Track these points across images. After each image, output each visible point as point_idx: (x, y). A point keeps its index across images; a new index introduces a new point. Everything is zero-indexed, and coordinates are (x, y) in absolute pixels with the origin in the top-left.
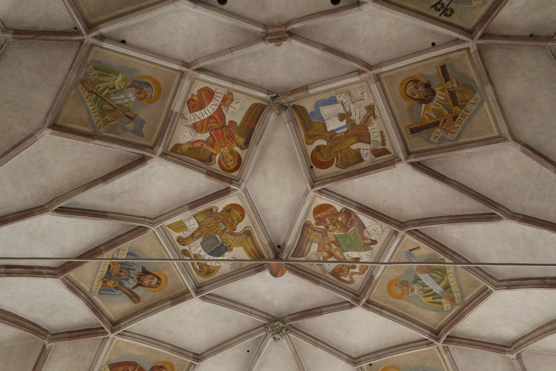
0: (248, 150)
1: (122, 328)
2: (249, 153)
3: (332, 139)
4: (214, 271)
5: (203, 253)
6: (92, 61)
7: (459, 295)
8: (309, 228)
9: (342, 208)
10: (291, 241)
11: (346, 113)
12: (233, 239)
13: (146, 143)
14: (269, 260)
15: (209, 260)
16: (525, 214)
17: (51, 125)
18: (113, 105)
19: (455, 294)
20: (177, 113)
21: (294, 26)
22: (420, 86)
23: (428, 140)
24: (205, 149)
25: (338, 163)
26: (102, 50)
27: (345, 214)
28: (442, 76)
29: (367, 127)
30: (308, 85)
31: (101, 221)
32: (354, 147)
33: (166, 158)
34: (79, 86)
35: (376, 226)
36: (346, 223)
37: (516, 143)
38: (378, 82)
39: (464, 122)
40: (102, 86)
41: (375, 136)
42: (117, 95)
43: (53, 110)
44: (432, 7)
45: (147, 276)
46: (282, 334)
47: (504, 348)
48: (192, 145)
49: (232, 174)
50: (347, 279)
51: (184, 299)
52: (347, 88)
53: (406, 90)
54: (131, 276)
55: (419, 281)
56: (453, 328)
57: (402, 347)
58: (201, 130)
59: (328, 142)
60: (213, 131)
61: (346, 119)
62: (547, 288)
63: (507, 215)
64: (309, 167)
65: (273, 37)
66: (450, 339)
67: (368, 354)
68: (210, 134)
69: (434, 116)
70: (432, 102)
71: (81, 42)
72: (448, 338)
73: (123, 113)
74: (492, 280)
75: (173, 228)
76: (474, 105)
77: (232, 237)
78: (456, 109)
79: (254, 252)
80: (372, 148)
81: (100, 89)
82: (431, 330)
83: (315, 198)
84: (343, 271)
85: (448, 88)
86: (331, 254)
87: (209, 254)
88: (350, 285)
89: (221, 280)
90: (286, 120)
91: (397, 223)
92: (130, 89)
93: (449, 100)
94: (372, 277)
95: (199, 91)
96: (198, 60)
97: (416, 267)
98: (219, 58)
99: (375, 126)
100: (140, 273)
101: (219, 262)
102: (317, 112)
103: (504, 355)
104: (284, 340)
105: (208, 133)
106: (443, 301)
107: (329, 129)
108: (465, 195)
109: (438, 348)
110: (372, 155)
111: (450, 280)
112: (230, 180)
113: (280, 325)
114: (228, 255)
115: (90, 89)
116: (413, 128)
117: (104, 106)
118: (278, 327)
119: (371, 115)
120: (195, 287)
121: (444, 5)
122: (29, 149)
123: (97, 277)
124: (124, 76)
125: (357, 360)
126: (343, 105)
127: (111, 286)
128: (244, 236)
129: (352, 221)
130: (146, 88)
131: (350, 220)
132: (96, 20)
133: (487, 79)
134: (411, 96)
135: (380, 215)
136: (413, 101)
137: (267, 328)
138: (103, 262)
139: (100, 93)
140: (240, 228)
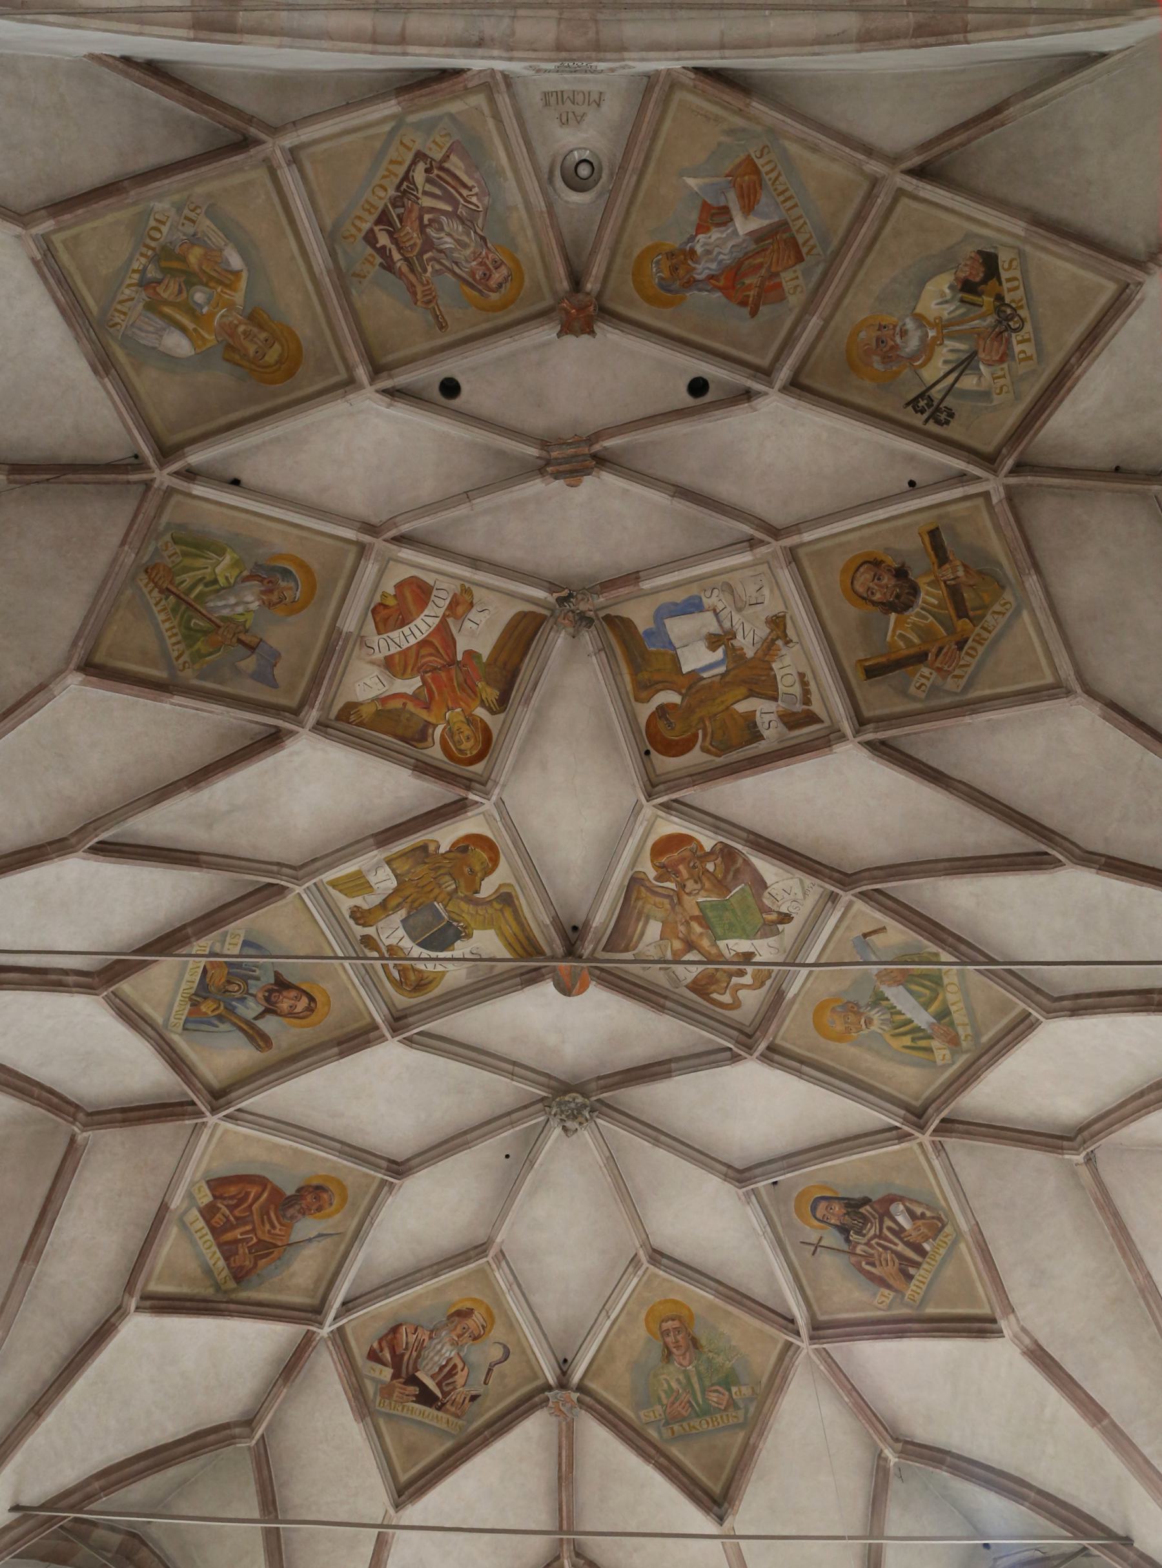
2: (508, 721)
3: (694, 690)
4: (430, 982)
5: (407, 943)
6: (168, 524)
7: (969, 1031)
8: (643, 889)
9: (715, 842)
10: (602, 917)
12: (474, 912)
13: (283, 701)
14: (553, 958)
15: (419, 959)
16: (1111, 854)
17: (82, 664)
18: (214, 619)
19: (960, 1030)
20: (349, 634)
21: (609, 443)
23: (904, 693)
24: (412, 714)
25: (707, 744)
26: (189, 501)
27: (722, 857)
28: (932, 553)
29: (769, 663)
30: (638, 572)
31: (185, 873)
32: (742, 707)
33: (326, 733)
34: (141, 580)
35: (791, 882)
36: (725, 877)
37: (1092, 699)
38: (793, 564)
39: (980, 653)
40: (188, 578)
41: (787, 684)
42: (222, 598)
43: (86, 632)
45: (285, 993)
46: (582, 1120)
47: (1059, 1142)
48: (383, 705)
49: (471, 768)
50: (726, 998)
51: (367, 1044)
52: (724, 578)
53: (855, 582)
54: (251, 991)
55: (884, 1003)
56: (954, 1103)
57: (845, 1144)
59: (684, 696)
60: (429, 674)
61: (723, 646)
62: (1154, 1011)
63: (1073, 855)
64: (643, 753)
65: (561, 468)
66: (949, 1126)
67: (770, 1162)
68: (423, 679)
69: (916, 640)
71: (146, 484)
72: (944, 1124)
73: (234, 634)
74: (1039, 998)
75: (341, 887)
76: (1001, 616)
77: (471, 908)
78: (962, 624)
79: (521, 943)
80: (781, 709)
81: (184, 584)
82: (907, 1108)
83: (654, 822)
84: (717, 982)
85: (945, 578)
86: (690, 946)
87: (420, 945)
89: (446, 1002)
90: (591, 649)
91: (836, 875)
92: (248, 584)
93: (949, 605)
94: (780, 995)
95: (399, 586)
96: (397, 519)
97: (875, 972)
98: (443, 513)
99: (787, 661)
100: (271, 987)
101: (445, 963)
102: (658, 632)
103: (1060, 1156)
104: (586, 1132)
105: (419, 678)
106: (935, 1044)
107: (685, 670)
108: (985, 814)
109: (921, 1145)
110: (781, 725)
111: (951, 998)
112: (465, 781)
113: (577, 1101)
114: (461, 948)
115: (165, 586)
116: (869, 666)
117: (193, 621)
118: (573, 1105)
120: (390, 1016)
121: (932, 401)
122: (36, 716)
123: (179, 995)
124: (235, 556)
125: (747, 1175)
126: (716, 614)
127: (209, 1013)
128: (497, 906)
129: (737, 871)
130: (283, 580)
131: (733, 869)
132: (179, 437)
133: (1028, 560)
134: (865, 595)
135: (798, 858)
136: (871, 607)
137: (550, 1107)
138: (191, 962)
139: (184, 593)
140: (488, 888)
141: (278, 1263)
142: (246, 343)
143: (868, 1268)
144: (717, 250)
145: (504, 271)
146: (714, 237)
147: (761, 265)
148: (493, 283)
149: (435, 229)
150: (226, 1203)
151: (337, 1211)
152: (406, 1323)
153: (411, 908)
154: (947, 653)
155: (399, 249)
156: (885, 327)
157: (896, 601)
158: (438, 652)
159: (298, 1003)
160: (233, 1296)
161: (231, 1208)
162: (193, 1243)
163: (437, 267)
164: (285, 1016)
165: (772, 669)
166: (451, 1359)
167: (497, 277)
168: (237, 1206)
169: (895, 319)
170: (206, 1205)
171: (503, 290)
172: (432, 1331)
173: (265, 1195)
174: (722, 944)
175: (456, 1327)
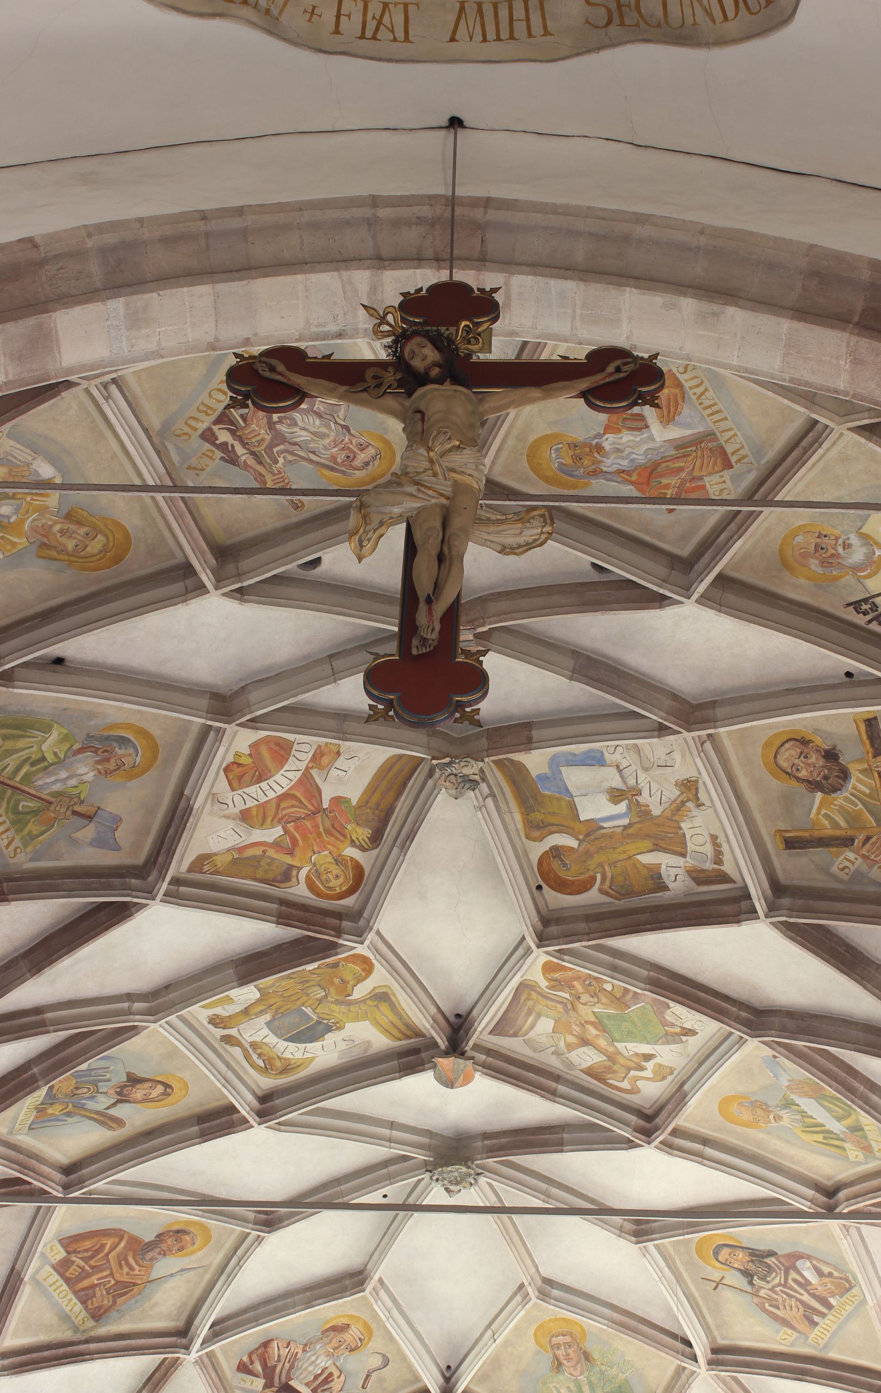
0: (381, 850)
1: (87, 1183)
3: (592, 837)
8: (533, 992)
11: (627, 788)
18: (43, 796)
22: (811, 753)
24: (273, 859)
28: (867, 742)
29: (677, 822)
32: (647, 859)
40: (12, 762)
42: (50, 774)
44: (849, 605)
45: (138, 1086)
48: (239, 853)
50: (625, 1085)
53: (779, 756)
58: (261, 823)
59: (581, 842)
60: (292, 824)
61: (627, 801)
64: (534, 889)
68: (284, 828)
69: (843, 824)
70: (839, 792)
77: (343, 1008)
79: (399, 1029)
88: (629, 1095)
92: (80, 756)
99: (698, 822)
100: (123, 1084)
105: (280, 828)
110: (688, 879)
118: (456, 1174)
119: (688, 800)
126: (620, 771)
130: (120, 748)
134: (789, 771)
136: (794, 782)
139: (9, 779)
141: (138, 1297)
142: (63, 540)
143: (771, 1309)
144: (628, 450)
145: (371, 451)
146: (624, 440)
147: (681, 469)
148: (357, 463)
149: (288, 425)
150: (80, 1256)
151: (200, 1249)
152: (277, 1339)
153: (276, 1012)
154: (876, 842)
155: (244, 445)
156: (825, 536)
157: (824, 782)
158: (301, 802)
159: (152, 1091)
160: (92, 1333)
161: (86, 1260)
162: (49, 1297)
163: (290, 458)
164: (139, 1102)
165: (681, 828)
166: (327, 1368)
167: (362, 457)
168: (92, 1257)
169: (837, 532)
170: (60, 1261)
171: (370, 467)
172: (306, 1345)
173: (123, 1244)
174: (620, 1046)
175: (331, 1341)
